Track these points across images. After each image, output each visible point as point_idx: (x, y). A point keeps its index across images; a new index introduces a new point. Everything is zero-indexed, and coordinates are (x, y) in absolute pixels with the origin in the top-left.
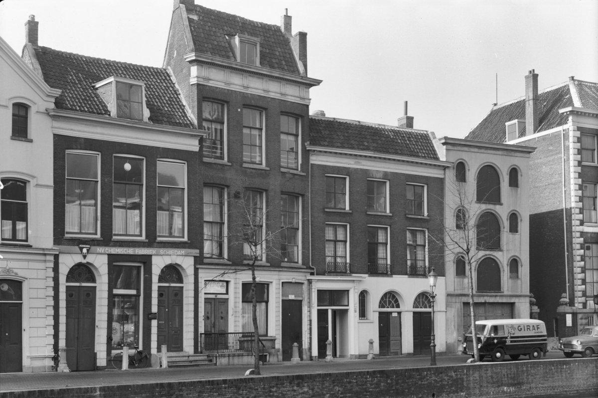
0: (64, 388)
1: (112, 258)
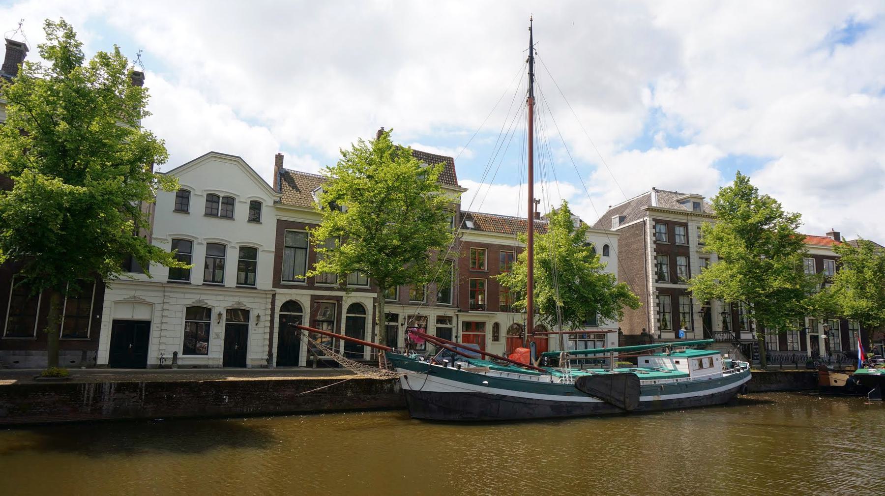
0: (378, 378)
1: (313, 297)
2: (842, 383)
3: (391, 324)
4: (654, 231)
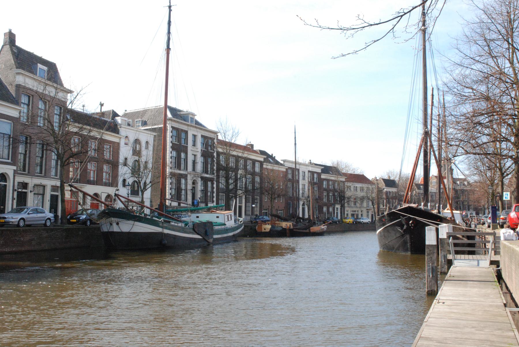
2: (268, 230)
3: (24, 190)
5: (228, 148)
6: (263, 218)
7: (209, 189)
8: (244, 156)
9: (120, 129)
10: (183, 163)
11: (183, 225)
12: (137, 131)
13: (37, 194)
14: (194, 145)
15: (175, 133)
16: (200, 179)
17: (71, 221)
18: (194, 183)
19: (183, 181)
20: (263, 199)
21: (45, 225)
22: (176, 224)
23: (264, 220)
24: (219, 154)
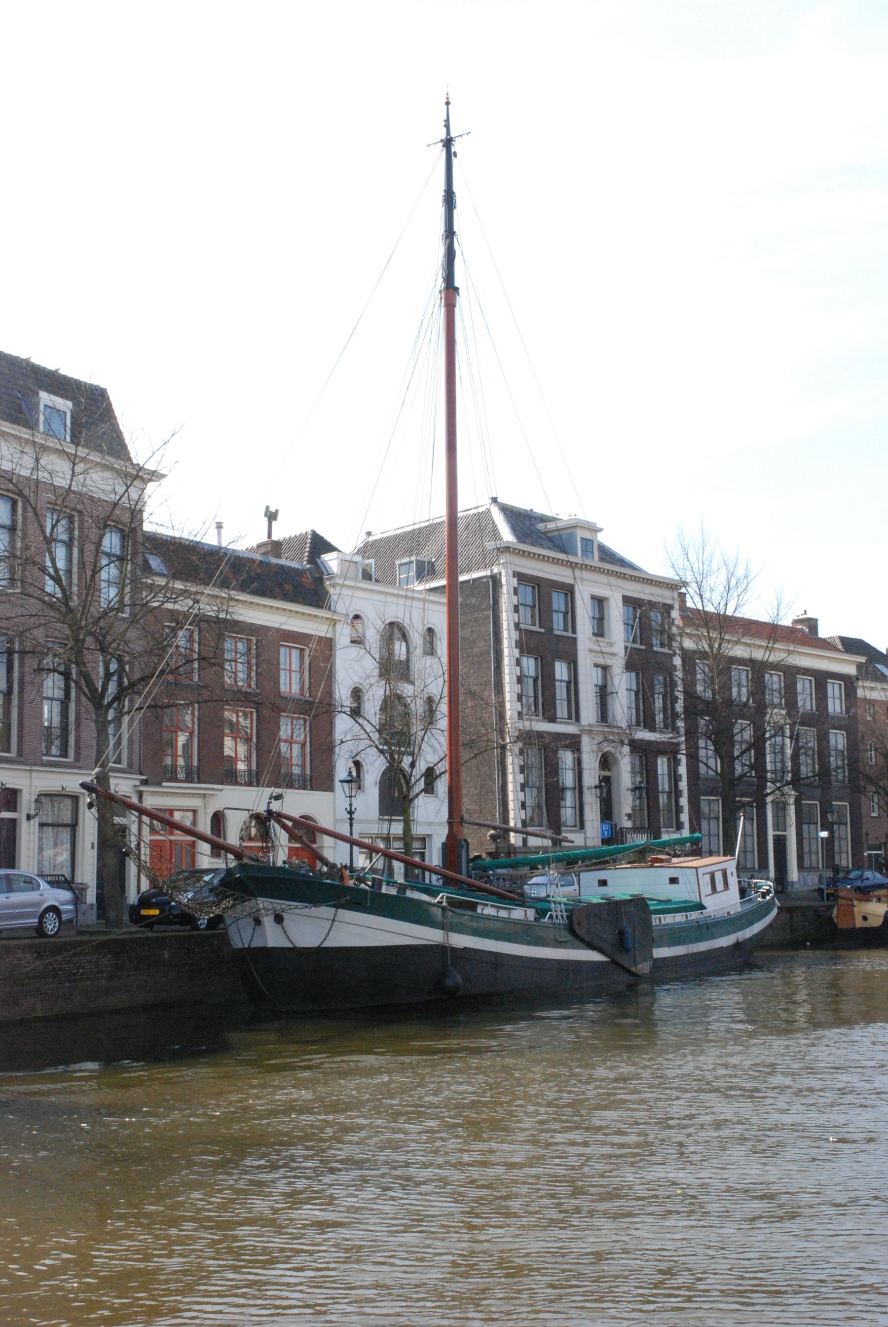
2: (876, 922)
4: (515, 601)
5: (714, 634)
6: (860, 878)
7: (664, 783)
8: (771, 659)
9: (331, 591)
10: (564, 696)
11: (531, 914)
12: (406, 597)
13: (52, 825)
14: (600, 631)
15: (527, 594)
16: (626, 749)
17: (144, 912)
18: (606, 762)
19: (567, 758)
20: (864, 811)
21: (40, 930)
22: (503, 914)
23: (866, 883)
24: (689, 658)
